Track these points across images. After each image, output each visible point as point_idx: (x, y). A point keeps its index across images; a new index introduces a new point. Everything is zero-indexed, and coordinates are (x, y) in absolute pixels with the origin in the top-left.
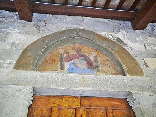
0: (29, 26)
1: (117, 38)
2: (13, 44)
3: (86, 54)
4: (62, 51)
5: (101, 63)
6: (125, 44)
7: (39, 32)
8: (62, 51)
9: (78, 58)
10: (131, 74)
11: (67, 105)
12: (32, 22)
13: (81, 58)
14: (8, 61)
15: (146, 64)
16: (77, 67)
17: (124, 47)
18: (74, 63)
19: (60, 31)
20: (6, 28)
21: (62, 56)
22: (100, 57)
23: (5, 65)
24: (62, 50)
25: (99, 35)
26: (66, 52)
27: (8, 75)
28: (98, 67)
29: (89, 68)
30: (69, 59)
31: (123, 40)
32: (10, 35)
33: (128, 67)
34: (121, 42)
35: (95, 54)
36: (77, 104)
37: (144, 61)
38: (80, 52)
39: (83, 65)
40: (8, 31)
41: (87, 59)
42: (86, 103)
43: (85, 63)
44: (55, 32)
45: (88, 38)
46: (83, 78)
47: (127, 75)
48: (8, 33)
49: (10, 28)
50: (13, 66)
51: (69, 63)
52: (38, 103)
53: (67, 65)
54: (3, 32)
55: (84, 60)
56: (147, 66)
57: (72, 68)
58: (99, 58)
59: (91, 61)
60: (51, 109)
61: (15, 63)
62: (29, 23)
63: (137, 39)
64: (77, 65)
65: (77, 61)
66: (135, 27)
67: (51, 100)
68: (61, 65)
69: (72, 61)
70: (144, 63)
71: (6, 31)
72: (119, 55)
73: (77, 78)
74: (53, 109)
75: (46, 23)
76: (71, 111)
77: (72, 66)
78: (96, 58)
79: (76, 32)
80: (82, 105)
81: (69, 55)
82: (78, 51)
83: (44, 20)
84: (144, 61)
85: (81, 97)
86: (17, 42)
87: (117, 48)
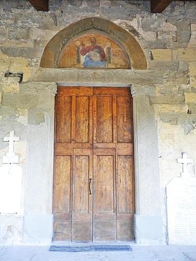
0: (47, 17)
1: (130, 27)
2: (35, 41)
3: (100, 45)
4: (78, 43)
5: (113, 55)
6: (137, 34)
7: (56, 25)
8: (78, 43)
9: (93, 50)
10: (136, 67)
11: (82, 94)
12: (49, 12)
13: (96, 50)
14: (35, 60)
15: (152, 56)
16: (91, 60)
17: (136, 38)
18: (89, 56)
19: (76, 21)
20: (27, 22)
21: (78, 48)
22: (113, 48)
23: (33, 64)
24: (78, 42)
25: (113, 24)
26: (83, 45)
27: (37, 72)
28: (110, 60)
29: (102, 61)
30: (84, 52)
31: (137, 29)
32: (126, 224)
33: (134, 60)
34: (134, 31)
35: (109, 44)
36: (90, 93)
37: (151, 54)
38: (95, 43)
39: (96, 57)
40: (29, 26)
41: (101, 51)
42: (97, 92)
43: (99, 55)
44: (72, 23)
45: (102, 29)
46: (95, 73)
47: (132, 69)
48: (29, 28)
49: (30, 22)
50: (39, 64)
51: (85, 56)
52: (62, 93)
53: (83, 59)
54: (25, 28)
55: (98, 52)
56: (152, 58)
57: (87, 61)
58: (112, 49)
59: (104, 53)
60: (71, 97)
61: (40, 61)
62: (46, 12)
63: (151, 26)
64: (92, 58)
65: (92, 53)
66: (153, 10)
67: (71, 91)
68: (78, 59)
69: (88, 54)
70: (150, 56)
71: (26, 26)
72: (129, 47)
73: (89, 74)
74: (73, 97)
75: (62, 12)
76: (85, 98)
77: (88, 59)
78: (109, 49)
79: (90, 23)
80: (94, 94)
81: (85, 48)
82: (93, 41)
83: (60, 8)
84: (151, 54)
85: (94, 87)
86: (39, 39)
87: (129, 40)
